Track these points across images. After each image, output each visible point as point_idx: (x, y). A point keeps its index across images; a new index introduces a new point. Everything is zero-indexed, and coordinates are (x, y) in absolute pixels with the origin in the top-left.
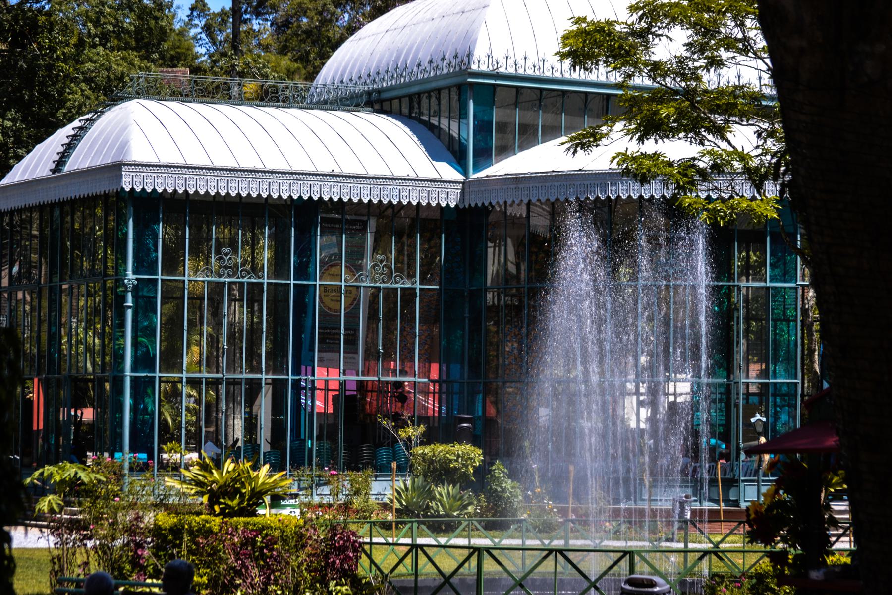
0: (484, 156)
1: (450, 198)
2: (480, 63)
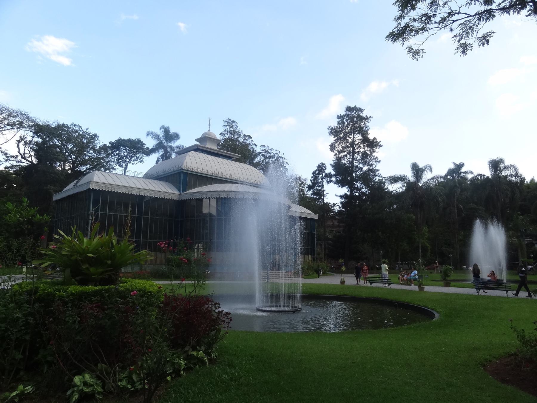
0: (184, 190)
1: (175, 198)
2: (185, 167)
